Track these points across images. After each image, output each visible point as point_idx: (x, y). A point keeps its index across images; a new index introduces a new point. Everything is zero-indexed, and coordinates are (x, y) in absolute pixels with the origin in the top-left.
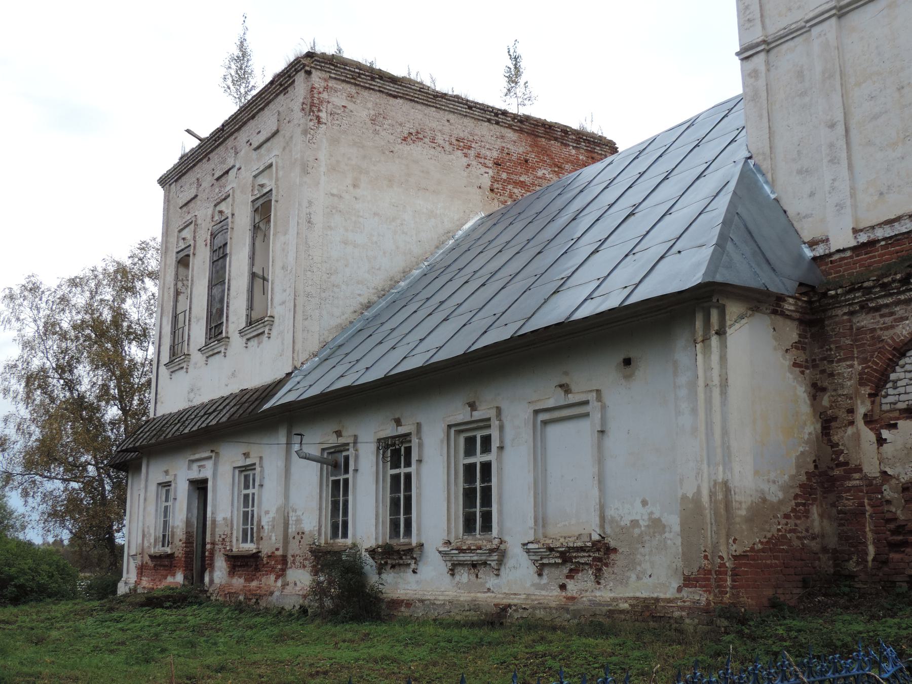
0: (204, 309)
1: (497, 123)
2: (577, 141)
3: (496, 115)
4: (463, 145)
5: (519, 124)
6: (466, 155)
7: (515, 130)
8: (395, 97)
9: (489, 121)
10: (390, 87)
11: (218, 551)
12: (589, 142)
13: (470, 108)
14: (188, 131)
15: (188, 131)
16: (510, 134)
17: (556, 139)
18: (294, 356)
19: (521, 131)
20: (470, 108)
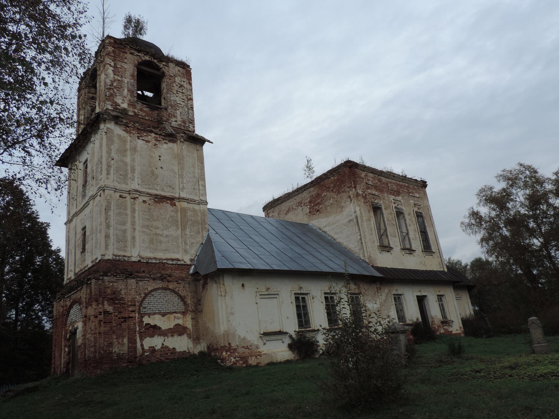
0: (163, 190)
1: (307, 189)
2: (332, 174)
3: (305, 187)
4: (300, 204)
5: (312, 184)
6: (301, 207)
7: (313, 187)
8: (282, 203)
9: (305, 190)
10: (279, 202)
11: (52, 83)
12: (335, 171)
13: (298, 191)
14: (212, 143)
15: (212, 143)
16: (312, 189)
17: (325, 179)
18: (91, 203)
19: (314, 185)
20: (298, 191)
